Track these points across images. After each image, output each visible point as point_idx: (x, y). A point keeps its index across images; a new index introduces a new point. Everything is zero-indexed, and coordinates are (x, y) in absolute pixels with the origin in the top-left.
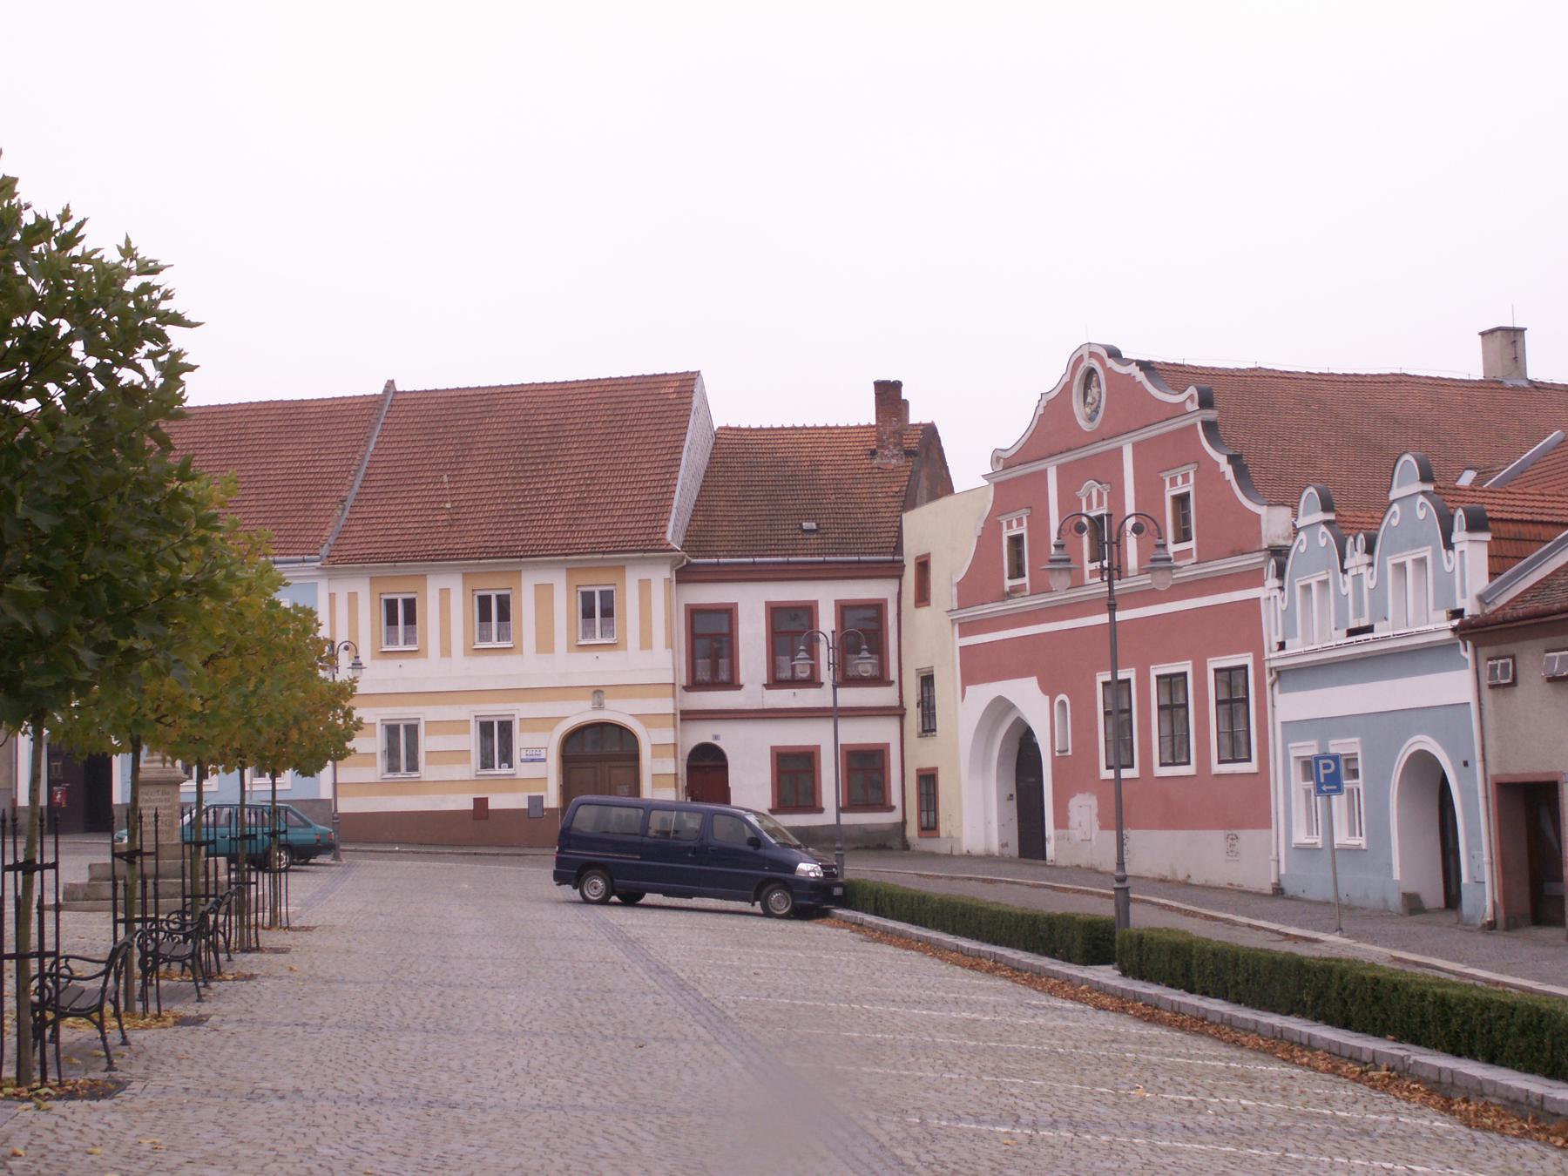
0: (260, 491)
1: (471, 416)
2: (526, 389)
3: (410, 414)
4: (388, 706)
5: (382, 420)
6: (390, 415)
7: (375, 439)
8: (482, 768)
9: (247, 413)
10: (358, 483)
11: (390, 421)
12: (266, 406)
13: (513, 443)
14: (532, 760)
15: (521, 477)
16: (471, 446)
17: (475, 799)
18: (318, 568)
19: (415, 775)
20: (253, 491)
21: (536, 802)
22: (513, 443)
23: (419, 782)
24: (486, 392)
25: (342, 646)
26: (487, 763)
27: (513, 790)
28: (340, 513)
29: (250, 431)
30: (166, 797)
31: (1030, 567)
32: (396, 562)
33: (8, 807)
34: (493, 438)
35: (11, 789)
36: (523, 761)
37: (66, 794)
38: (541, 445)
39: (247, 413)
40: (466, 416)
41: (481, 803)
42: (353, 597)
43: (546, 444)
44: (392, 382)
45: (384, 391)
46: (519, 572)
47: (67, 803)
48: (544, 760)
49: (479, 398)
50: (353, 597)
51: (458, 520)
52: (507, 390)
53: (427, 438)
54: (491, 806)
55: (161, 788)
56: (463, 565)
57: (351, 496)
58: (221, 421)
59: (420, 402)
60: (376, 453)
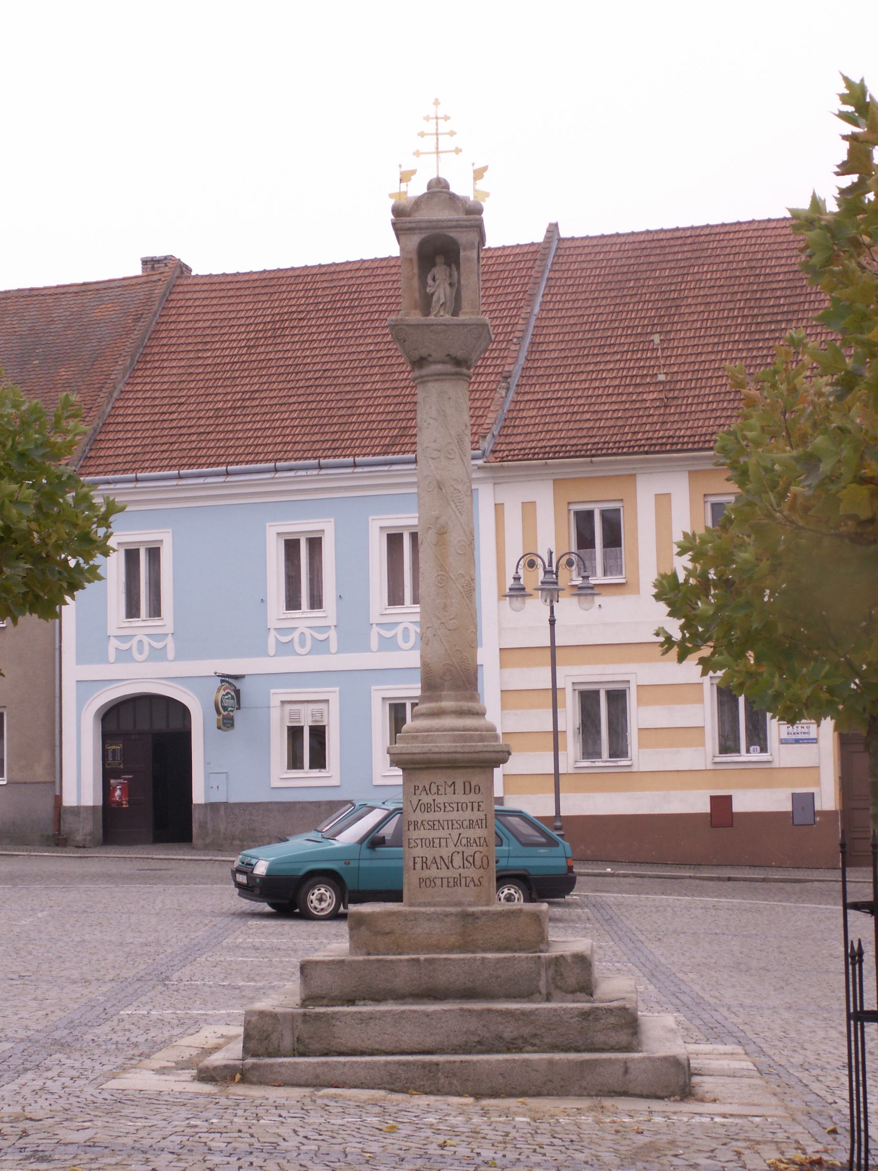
0: (385, 369)
1: (673, 265)
2: (744, 227)
3: (585, 265)
4: (584, 664)
5: (546, 275)
6: (556, 267)
7: (539, 299)
8: (720, 753)
9: (360, 273)
10: (523, 354)
11: (558, 275)
12: (384, 264)
13: (739, 296)
14: (797, 741)
15: (758, 340)
16: (678, 303)
17: (793, 794)
18: (480, 468)
19: (623, 762)
20: (376, 370)
21: (803, 801)
22: (739, 296)
23: (629, 773)
24: (688, 234)
25: (564, 560)
26: (728, 745)
27: (769, 784)
28: (503, 393)
29: (365, 295)
30: (473, 797)
31: (8, 769)
32: (593, 456)
33: (46, 808)
34: (706, 291)
35: (54, 782)
36: (783, 742)
37: (129, 790)
38: (779, 297)
39: (360, 273)
40: (664, 265)
41: (721, 803)
42: (529, 508)
43: (786, 297)
44: (556, 225)
45: (546, 237)
46: (633, 476)
47: (129, 802)
48: (815, 741)
49: (680, 242)
50: (529, 508)
51: (674, 398)
52: (718, 230)
53: (612, 294)
54: (738, 806)
55: (460, 778)
56: (694, 458)
57: (517, 371)
58: (325, 285)
59: (597, 249)
60: (544, 315)
